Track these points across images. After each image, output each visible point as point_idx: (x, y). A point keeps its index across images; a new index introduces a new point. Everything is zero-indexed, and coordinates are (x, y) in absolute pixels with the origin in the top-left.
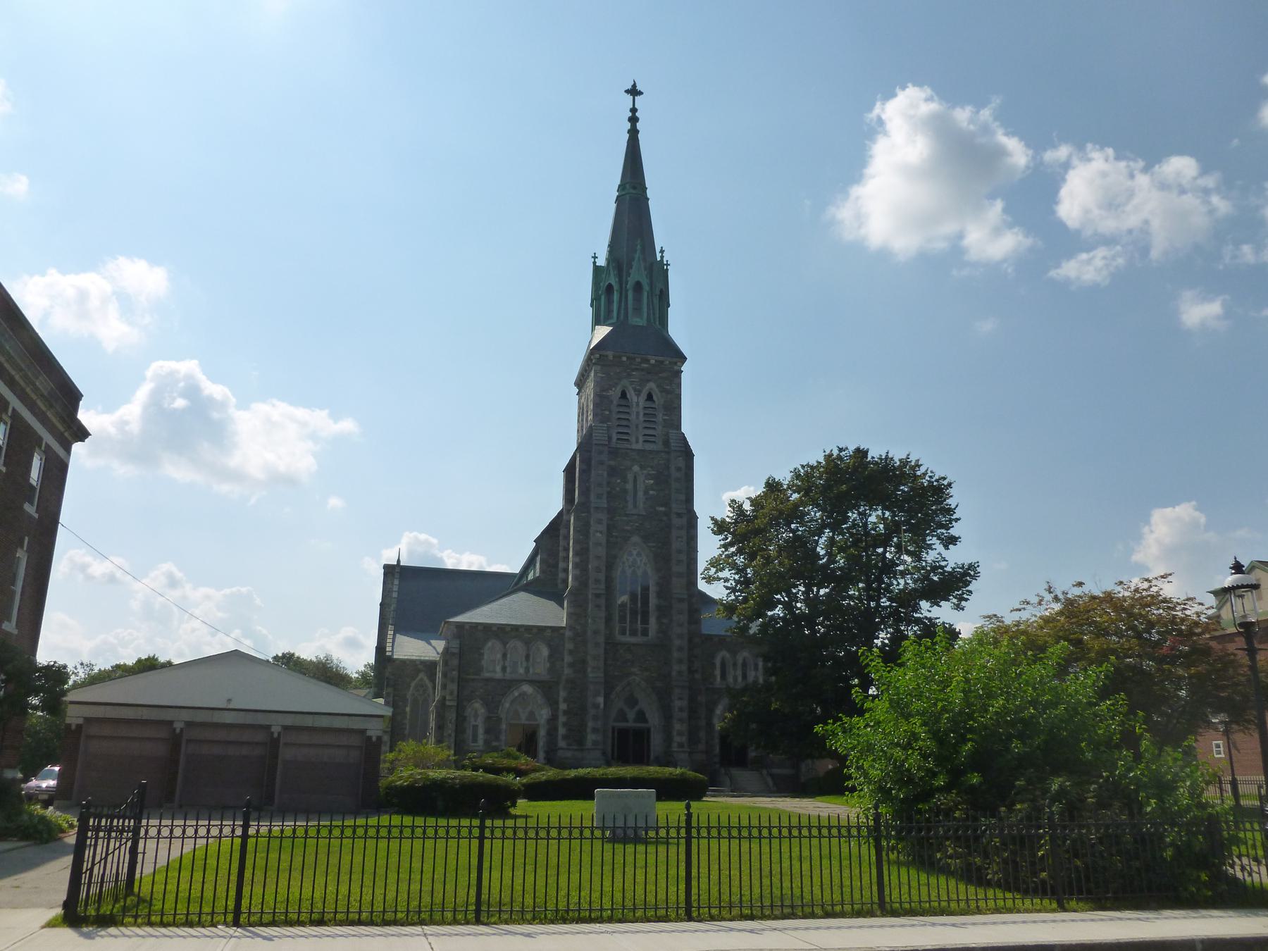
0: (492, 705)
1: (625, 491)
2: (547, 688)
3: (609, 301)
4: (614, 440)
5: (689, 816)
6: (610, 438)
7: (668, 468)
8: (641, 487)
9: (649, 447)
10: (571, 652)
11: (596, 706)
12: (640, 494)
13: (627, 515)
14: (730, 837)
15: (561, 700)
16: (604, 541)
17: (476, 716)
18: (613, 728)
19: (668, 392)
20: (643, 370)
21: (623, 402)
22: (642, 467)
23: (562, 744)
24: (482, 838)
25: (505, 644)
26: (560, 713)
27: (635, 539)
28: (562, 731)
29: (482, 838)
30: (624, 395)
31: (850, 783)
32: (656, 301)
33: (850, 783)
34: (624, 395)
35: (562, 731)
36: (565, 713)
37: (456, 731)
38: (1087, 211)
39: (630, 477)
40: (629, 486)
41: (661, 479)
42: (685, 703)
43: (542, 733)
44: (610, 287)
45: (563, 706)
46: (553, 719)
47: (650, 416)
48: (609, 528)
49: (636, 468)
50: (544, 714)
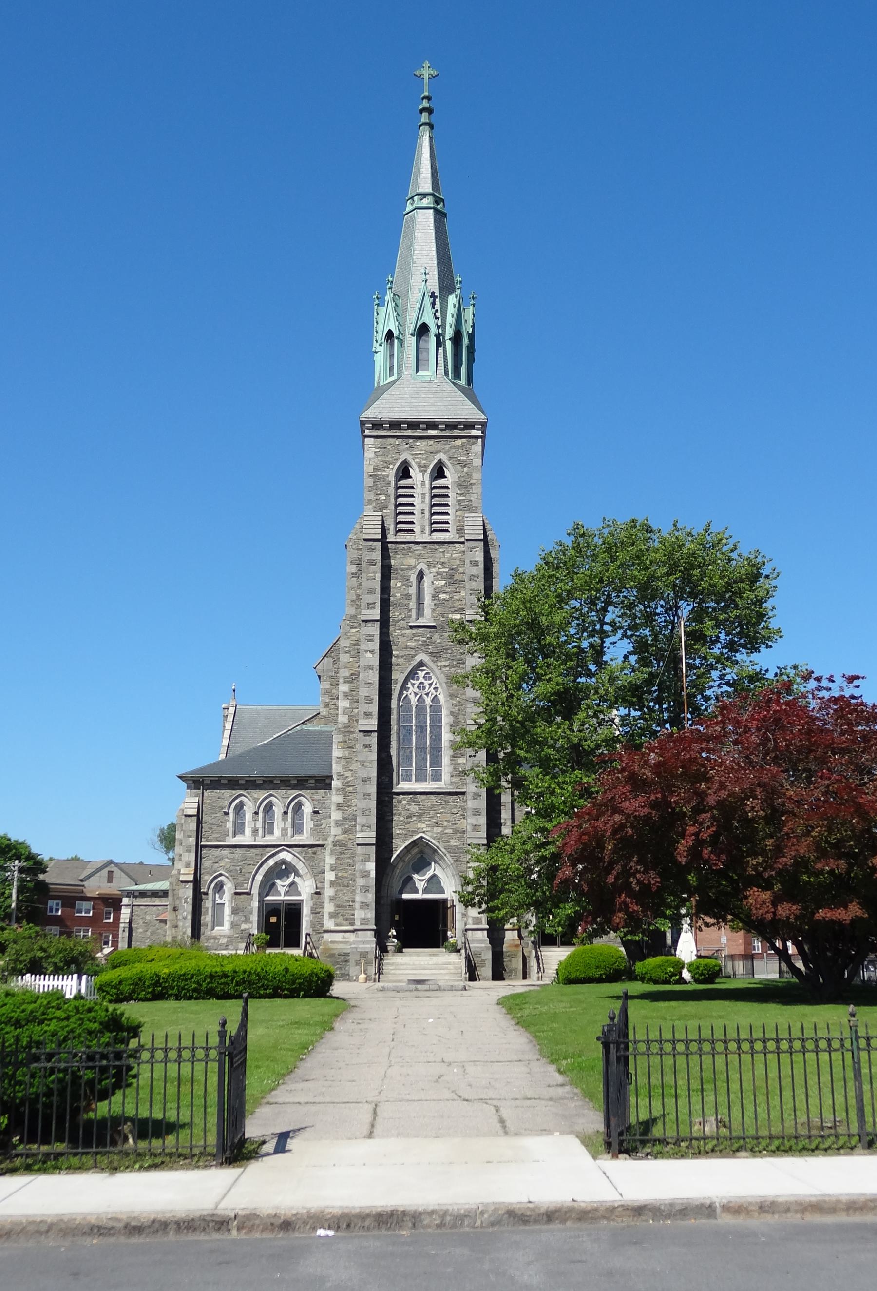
5: (853, 1028)
10: (339, 807)
11: (366, 874)
14: (778, 1051)
15: (327, 868)
22: (429, 565)
31: (60, 988)
33: (60, 988)
36: (332, 884)
40: (413, 590)
43: (306, 911)
45: (330, 876)
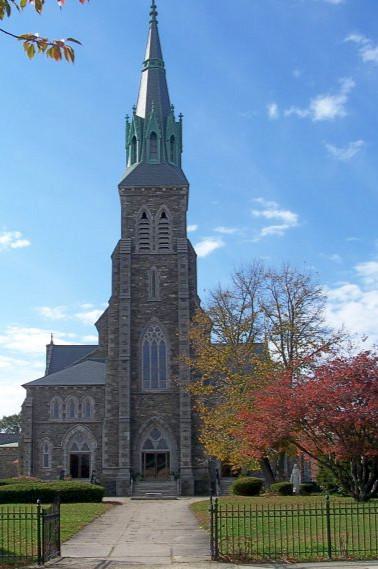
0: (56, 440)
1: (146, 285)
2: (94, 427)
3: (134, 150)
4: (137, 248)
6: (133, 249)
7: (176, 266)
8: (158, 282)
9: (163, 251)
11: (124, 439)
12: (157, 286)
13: (148, 302)
15: (103, 435)
16: (129, 323)
17: (47, 448)
18: (143, 454)
19: (176, 211)
20: (157, 196)
21: (144, 221)
22: (158, 267)
23: (104, 465)
24: (328, 515)
25: (64, 399)
26: (103, 445)
27: (154, 319)
28: (105, 456)
29: (328, 515)
30: (144, 216)
32: (168, 144)
34: (144, 216)
35: (105, 456)
37: (32, 458)
38: (337, 105)
39: (150, 275)
41: (172, 275)
42: (188, 434)
43: (92, 458)
44: (154, 135)
45: (105, 439)
46: (99, 448)
47: (163, 228)
48: (133, 311)
49: (154, 268)
50: (93, 445)
